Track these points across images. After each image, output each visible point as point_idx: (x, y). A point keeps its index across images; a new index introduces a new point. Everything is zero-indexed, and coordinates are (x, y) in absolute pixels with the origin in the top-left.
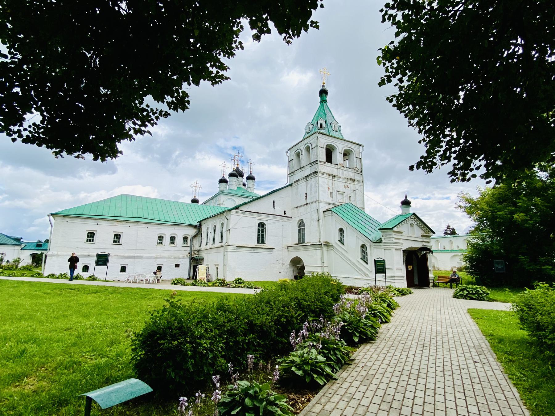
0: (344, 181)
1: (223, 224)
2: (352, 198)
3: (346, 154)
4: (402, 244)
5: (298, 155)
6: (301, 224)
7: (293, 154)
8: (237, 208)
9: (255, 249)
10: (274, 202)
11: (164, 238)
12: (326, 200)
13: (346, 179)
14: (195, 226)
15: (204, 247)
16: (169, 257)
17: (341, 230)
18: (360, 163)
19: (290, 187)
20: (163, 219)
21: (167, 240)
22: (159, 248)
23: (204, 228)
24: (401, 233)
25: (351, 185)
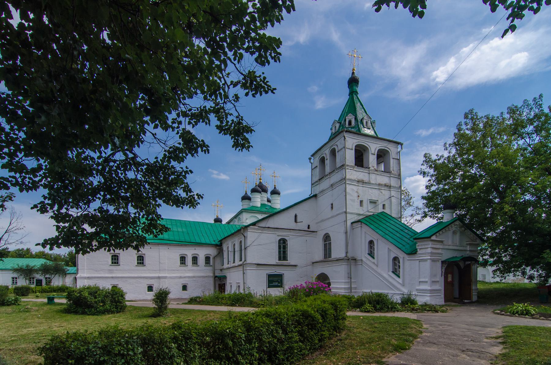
1: (241, 242)
2: (386, 206)
3: (382, 155)
4: (441, 254)
5: (323, 160)
6: (327, 238)
7: (316, 161)
8: (254, 224)
10: (296, 216)
12: (356, 211)
14: (216, 246)
15: (226, 266)
16: (194, 277)
17: (371, 242)
19: (313, 199)
20: (183, 239)
21: (189, 261)
23: (225, 248)
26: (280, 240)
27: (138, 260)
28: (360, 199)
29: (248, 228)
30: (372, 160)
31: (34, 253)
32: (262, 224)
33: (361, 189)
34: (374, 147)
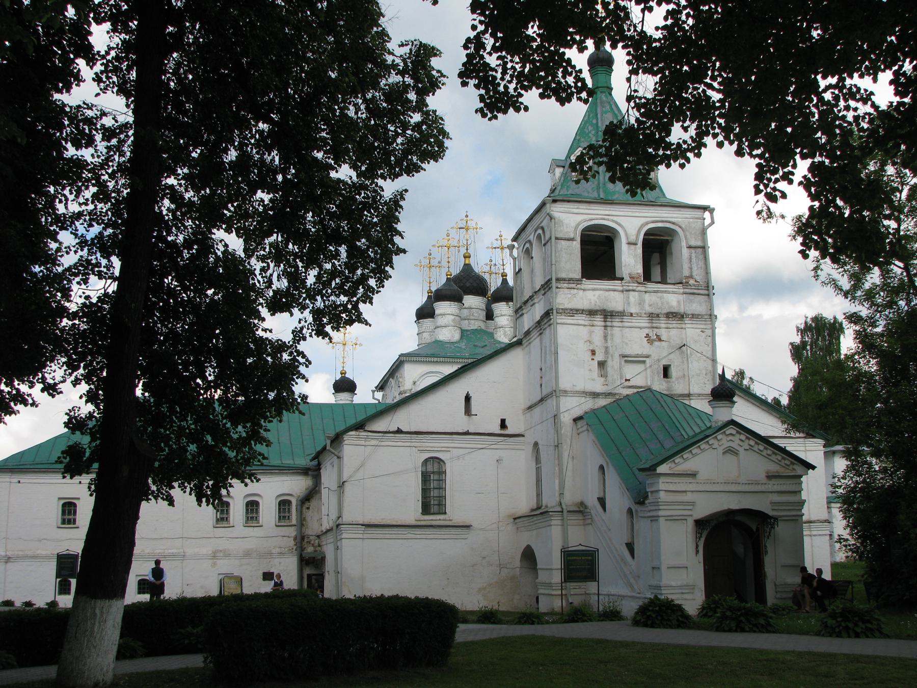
0: (644, 323)
2: (674, 371)
4: (693, 504)
9: (418, 531)
10: (468, 399)
11: (60, 521)
13: (653, 316)
18: (701, 263)
22: (220, 532)
24: (694, 475)
25: (671, 333)
29: (346, 437)
30: (629, 259)
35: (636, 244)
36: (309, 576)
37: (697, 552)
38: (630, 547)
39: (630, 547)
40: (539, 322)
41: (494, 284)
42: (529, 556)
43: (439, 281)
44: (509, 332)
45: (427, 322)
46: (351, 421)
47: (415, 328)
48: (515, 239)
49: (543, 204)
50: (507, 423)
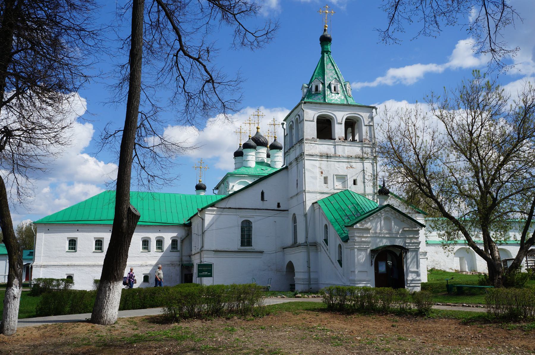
3: (351, 124)
10: (263, 193)
12: (318, 189)
14: (185, 225)
21: (153, 245)
26: (243, 222)
27: (96, 244)
28: (324, 175)
30: (339, 130)
31: (24, 251)
32: (223, 205)
33: (324, 164)
34: (340, 117)
35: (341, 124)
36: (185, 274)
37: (372, 264)
38: (340, 262)
39: (340, 262)
40: (293, 147)
41: (270, 141)
42: (290, 267)
43: (245, 140)
44: (282, 164)
45: (239, 158)
46: (210, 202)
47: (233, 161)
48: (285, 120)
49: (300, 104)
50: (281, 205)
